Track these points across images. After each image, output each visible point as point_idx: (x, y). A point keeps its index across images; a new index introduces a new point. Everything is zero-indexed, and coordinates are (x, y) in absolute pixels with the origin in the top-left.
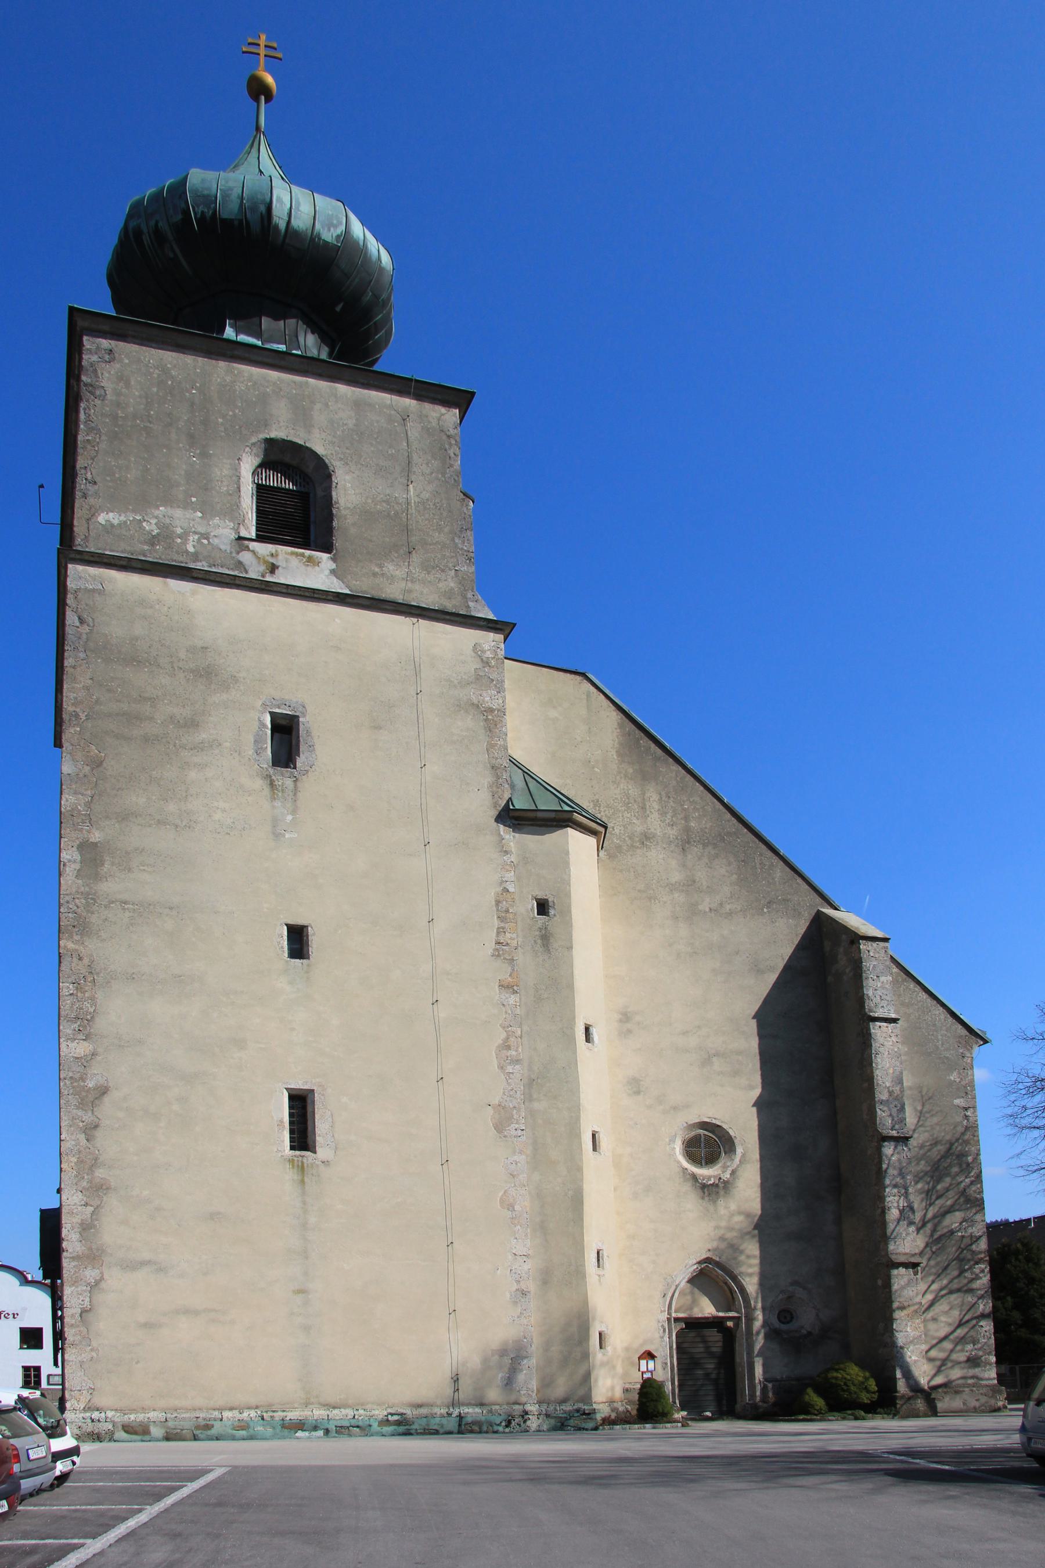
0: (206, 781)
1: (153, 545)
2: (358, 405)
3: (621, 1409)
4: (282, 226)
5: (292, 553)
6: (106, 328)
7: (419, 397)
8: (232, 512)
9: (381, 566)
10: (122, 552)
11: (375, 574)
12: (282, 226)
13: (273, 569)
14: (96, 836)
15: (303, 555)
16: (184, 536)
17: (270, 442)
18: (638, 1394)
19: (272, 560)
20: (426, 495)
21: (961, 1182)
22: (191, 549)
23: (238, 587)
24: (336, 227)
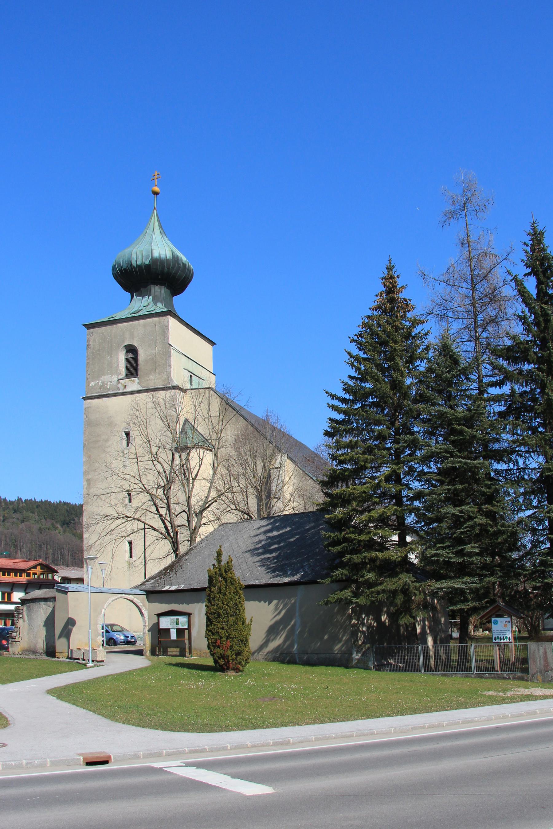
0: (8, 528)
1: (100, 389)
2: (145, 325)
3: (321, 501)
4: (135, 266)
5: (130, 380)
6: (90, 326)
7: (159, 316)
8: (117, 372)
9: (149, 377)
10: (97, 393)
11: (147, 380)
12: (135, 266)
13: (125, 387)
14: (90, 477)
15: (131, 380)
16: (107, 384)
17: (126, 347)
18: (188, 604)
19: (125, 384)
20: (160, 349)
21: (439, 404)
22: (108, 387)
23: (117, 396)
24: (148, 258)
